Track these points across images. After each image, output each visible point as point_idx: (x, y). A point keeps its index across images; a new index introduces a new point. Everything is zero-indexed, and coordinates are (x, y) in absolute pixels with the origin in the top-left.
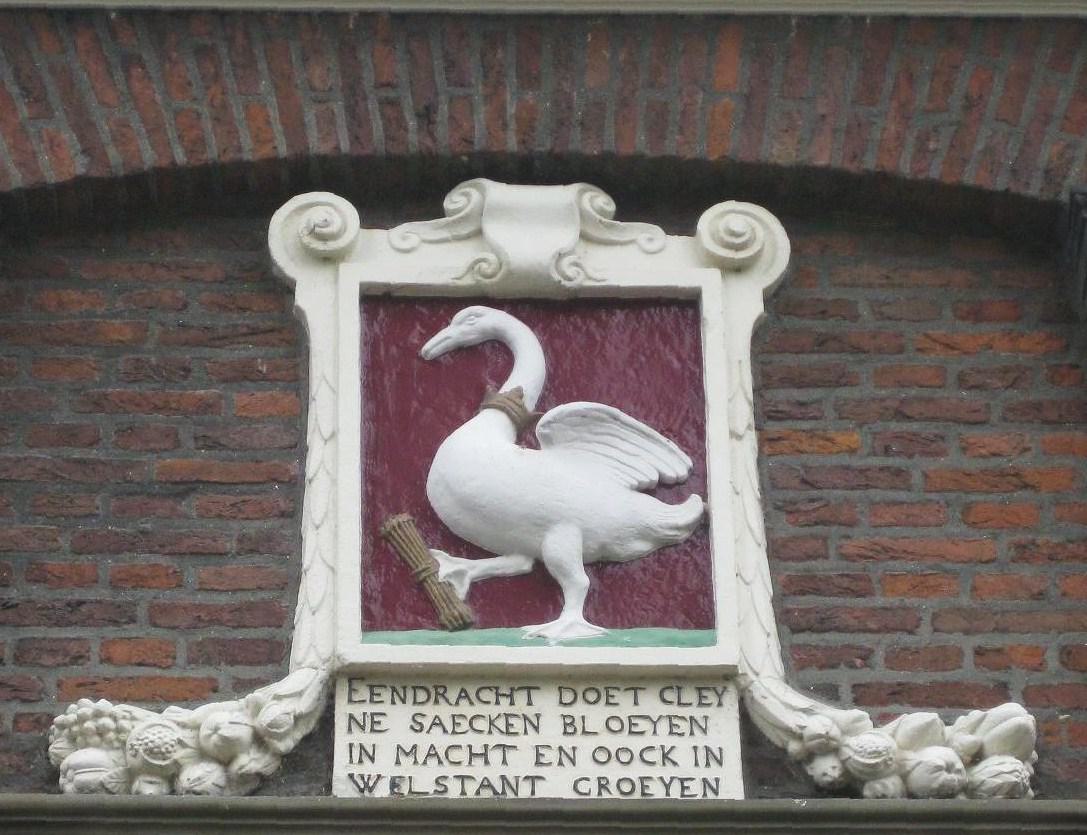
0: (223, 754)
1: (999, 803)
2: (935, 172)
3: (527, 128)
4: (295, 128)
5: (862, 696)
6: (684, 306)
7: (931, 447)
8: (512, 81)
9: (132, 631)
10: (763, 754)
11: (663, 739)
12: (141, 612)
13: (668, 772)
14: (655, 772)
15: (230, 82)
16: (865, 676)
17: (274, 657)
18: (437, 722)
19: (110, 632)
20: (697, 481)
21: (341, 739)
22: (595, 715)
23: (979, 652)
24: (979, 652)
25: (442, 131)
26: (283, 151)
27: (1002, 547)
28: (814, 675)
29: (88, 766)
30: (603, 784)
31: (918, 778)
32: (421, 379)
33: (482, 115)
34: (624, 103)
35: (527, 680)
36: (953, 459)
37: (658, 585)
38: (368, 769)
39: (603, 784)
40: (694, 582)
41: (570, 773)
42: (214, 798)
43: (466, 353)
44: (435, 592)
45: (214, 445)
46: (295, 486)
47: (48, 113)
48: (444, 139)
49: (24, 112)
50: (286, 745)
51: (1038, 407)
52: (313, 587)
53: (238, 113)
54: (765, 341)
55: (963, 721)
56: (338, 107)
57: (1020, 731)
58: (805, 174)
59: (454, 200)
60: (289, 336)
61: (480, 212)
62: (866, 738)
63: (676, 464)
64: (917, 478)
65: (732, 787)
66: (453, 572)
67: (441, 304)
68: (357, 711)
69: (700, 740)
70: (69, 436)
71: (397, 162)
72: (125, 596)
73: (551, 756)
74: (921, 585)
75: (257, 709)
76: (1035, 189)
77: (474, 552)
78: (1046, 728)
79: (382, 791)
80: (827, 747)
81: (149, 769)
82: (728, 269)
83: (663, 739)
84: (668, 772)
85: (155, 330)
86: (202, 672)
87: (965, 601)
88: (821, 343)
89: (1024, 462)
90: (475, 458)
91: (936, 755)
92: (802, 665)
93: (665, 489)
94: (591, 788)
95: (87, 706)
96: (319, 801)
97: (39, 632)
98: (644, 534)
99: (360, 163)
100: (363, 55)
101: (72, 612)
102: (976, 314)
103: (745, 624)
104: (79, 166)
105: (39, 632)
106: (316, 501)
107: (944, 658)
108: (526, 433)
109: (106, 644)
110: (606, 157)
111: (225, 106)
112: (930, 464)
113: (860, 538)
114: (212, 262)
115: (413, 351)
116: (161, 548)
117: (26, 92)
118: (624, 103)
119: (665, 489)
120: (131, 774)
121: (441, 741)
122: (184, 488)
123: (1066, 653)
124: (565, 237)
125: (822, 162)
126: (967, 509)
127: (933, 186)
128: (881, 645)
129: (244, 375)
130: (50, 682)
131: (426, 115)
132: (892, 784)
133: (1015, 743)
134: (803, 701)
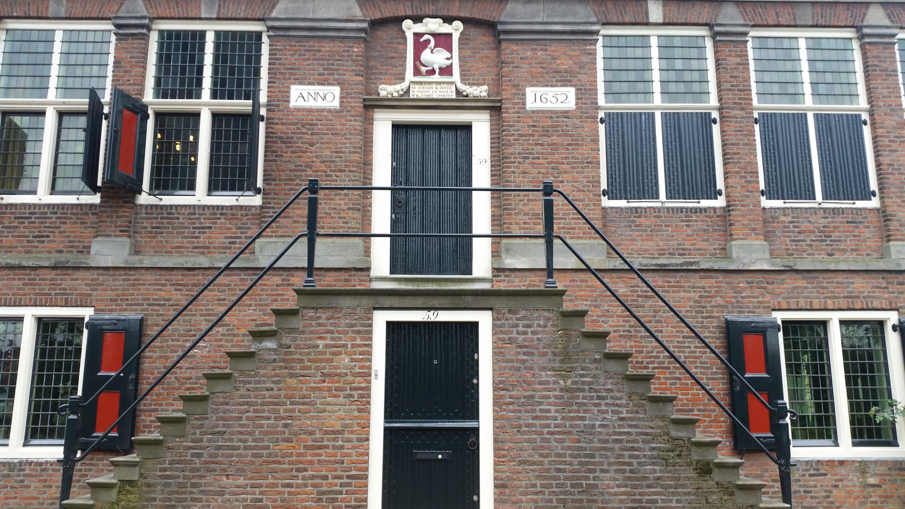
4: (405, 11)
5: (469, 84)
6: (451, 35)
7: (478, 53)
10: (458, 92)
17: (403, 79)
22: (439, 87)
29: (383, 93)
32: (420, 45)
35: (431, 83)
37: (446, 71)
43: (425, 41)
46: (405, 58)
48: (423, 13)
54: (460, 39)
60: (405, 38)
63: (449, 56)
65: (454, 96)
66: (423, 69)
67: (422, 35)
70: (379, 51)
76: (492, 20)
82: (456, 29)
90: (426, 55)
93: (448, 59)
101: (380, 74)
103: (456, 76)
104: (380, 16)
107: (478, 80)
114: (395, 28)
119: (448, 59)
129: (399, 43)
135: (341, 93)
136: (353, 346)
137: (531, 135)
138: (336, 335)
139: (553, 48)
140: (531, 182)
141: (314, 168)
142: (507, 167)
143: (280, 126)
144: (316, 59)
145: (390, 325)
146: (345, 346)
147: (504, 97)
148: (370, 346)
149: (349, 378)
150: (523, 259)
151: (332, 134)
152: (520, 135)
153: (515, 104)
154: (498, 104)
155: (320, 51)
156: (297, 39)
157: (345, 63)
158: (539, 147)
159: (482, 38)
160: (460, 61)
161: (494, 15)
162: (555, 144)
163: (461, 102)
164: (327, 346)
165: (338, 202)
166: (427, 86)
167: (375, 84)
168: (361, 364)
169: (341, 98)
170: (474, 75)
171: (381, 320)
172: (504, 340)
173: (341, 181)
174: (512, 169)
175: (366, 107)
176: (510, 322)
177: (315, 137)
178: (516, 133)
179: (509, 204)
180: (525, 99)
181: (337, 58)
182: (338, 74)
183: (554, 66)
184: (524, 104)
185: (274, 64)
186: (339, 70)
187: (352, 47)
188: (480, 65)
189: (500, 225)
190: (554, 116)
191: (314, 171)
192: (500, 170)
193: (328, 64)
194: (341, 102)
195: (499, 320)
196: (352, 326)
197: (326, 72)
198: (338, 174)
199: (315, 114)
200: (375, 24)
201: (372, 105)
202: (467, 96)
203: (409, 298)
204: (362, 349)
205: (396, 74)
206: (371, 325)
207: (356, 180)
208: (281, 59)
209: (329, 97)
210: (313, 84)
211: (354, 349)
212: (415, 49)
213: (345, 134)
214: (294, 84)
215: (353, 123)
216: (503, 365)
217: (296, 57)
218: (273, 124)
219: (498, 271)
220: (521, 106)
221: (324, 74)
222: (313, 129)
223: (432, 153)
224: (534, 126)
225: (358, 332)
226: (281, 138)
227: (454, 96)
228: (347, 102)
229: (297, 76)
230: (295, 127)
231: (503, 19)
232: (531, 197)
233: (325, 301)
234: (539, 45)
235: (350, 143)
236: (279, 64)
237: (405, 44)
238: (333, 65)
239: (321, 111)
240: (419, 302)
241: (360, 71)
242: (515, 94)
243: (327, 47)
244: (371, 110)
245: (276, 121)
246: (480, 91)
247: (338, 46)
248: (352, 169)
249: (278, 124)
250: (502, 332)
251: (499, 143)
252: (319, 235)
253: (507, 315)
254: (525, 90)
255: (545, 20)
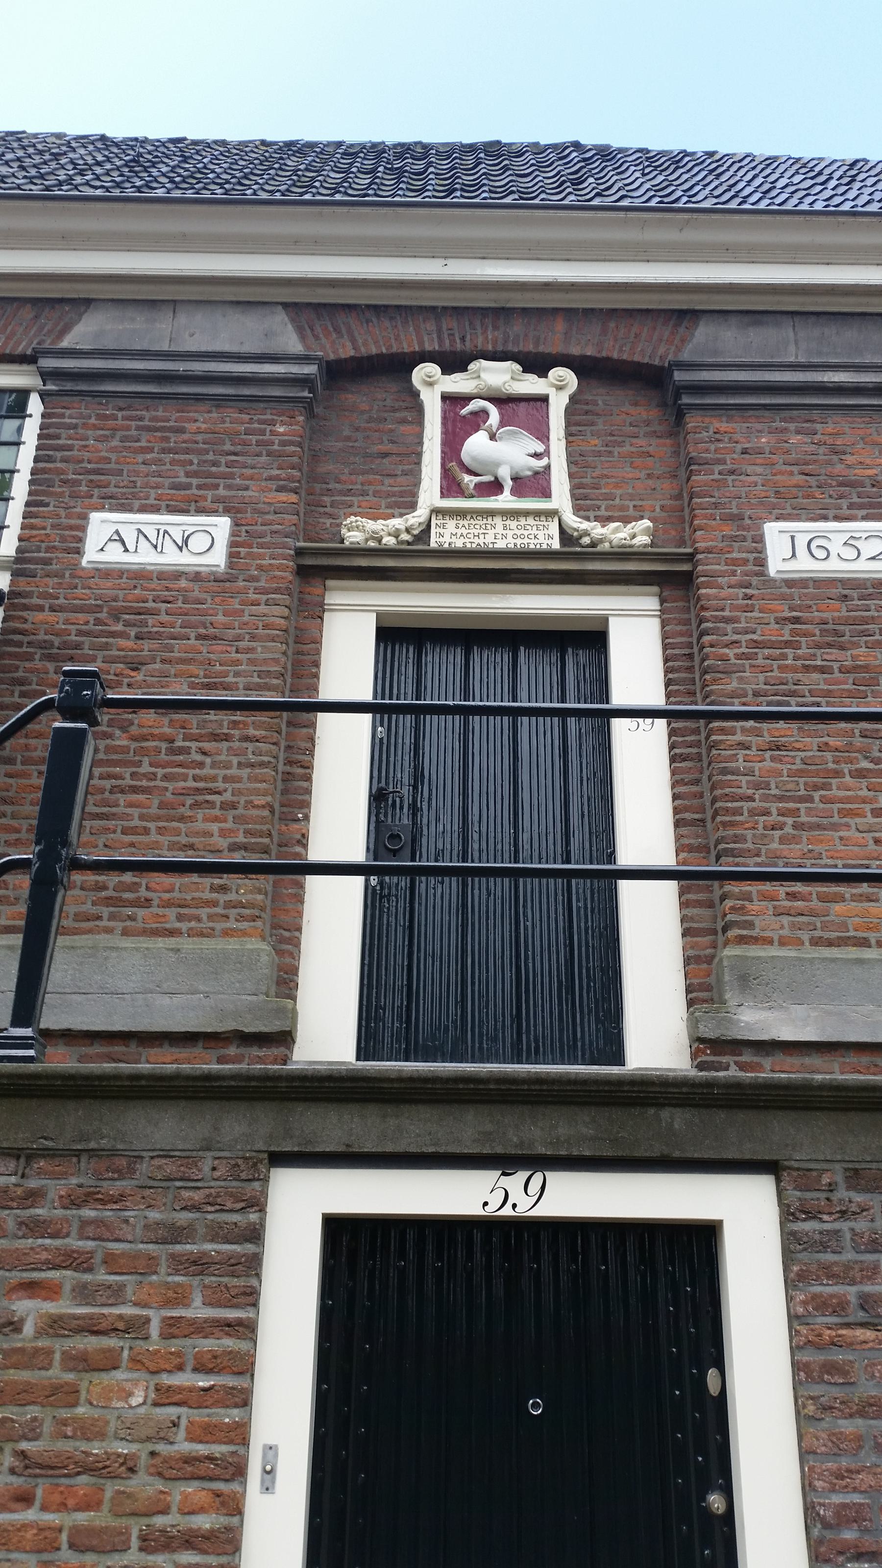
0: (396, 534)
1: (641, 549)
2: (625, 357)
3: (495, 342)
4: (421, 343)
5: (597, 519)
6: (544, 399)
7: (620, 444)
8: (490, 328)
9: (367, 498)
10: (565, 535)
11: (534, 531)
12: (370, 493)
13: (536, 541)
14: (532, 541)
15: (400, 328)
16: (598, 513)
17: (412, 506)
18: (463, 526)
19: (361, 498)
20: (547, 453)
21: (433, 530)
22: (513, 524)
23: (634, 506)
24: (634, 506)
25: (468, 343)
26: (417, 349)
27: (643, 475)
28: (582, 513)
29: (353, 537)
30: (515, 545)
31: (615, 542)
32: (460, 421)
33: (480, 339)
34: (526, 335)
35: (491, 513)
36: (627, 448)
37: (533, 484)
38: (441, 539)
39: (515, 545)
40: (545, 484)
41: (505, 542)
42: (394, 547)
44: (463, 486)
45: (393, 442)
46: (419, 455)
47: (342, 337)
48: (469, 346)
49: (334, 336)
50: (416, 532)
51: (655, 432)
52: (425, 484)
53: (402, 337)
54: (569, 412)
55: (630, 526)
56: (435, 336)
57: (649, 527)
58: (584, 357)
59: (471, 367)
60: (418, 409)
61: (479, 369)
62: (597, 530)
63: (540, 448)
64: (616, 454)
65: (556, 545)
67: (466, 399)
68: (438, 522)
69: (546, 531)
70: (348, 439)
71: (454, 353)
72: (366, 488)
73: (499, 536)
74: (617, 486)
75: (407, 520)
76: (657, 362)
77: (476, 475)
78: (656, 529)
79: (446, 546)
80: (586, 533)
81: (373, 538)
82: (559, 387)
83: (534, 531)
84: (536, 541)
85: (376, 407)
86: (390, 511)
87: (630, 491)
88: (587, 413)
89: (650, 449)
90: (477, 445)
91: (621, 535)
92: (578, 510)
93: (537, 456)
94: (511, 546)
95: (353, 518)
96: (426, 547)
97: (338, 498)
98: (530, 469)
99: (440, 353)
100: (443, 320)
102: (636, 404)
103: (561, 496)
104: (352, 353)
105: (338, 498)
106: (426, 458)
107: (623, 508)
108: (493, 437)
109: (359, 501)
110: (519, 352)
111: (398, 335)
112: (620, 449)
113: (597, 472)
114: (393, 387)
115: (457, 414)
116: (377, 473)
117: (335, 330)
118: (526, 335)
119: (537, 456)
120: (367, 540)
121: (465, 532)
122: (385, 455)
123: (662, 507)
124: (507, 377)
125: (589, 354)
126: (632, 463)
127: (624, 362)
128: (603, 504)
129: (404, 421)
130: (342, 513)
131: (463, 339)
132: (607, 545)
133: (646, 531)
134: (579, 520)
135: (233, 534)
136: (173, 1328)
137: (787, 644)
138: (102, 1276)
139: (830, 428)
140: (800, 773)
141: (134, 730)
142: (723, 731)
143: (40, 616)
144: (170, 451)
145: (339, 1232)
146: (134, 1328)
147: (700, 545)
148: (247, 1329)
149: (143, 1485)
150: (799, 1010)
151: (199, 637)
152: (756, 644)
153: (735, 562)
154: (686, 567)
155: (181, 430)
156: (121, 402)
157: (249, 461)
158: (815, 676)
159: (629, 410)
160: (570, 463)
161: (661, 351)
162: (866, 668)
163: (572, 565)
164: (55, 1326)
165: (200, 825)
166: (480, 522)
167: (331, 516)
168: (200, 1416)
169: (232, 544)
170: (610, 497)
171: (300, 1207)
172: (839, 1307)
173: (214, 765)
174: (739, 737)
175: (305, 573)
176: (861, 1225)
177: (146, 645)
178: (744, 638)
179: (737, 839)
180: (762, 551)
181: (228, 447)
182: (229, 487)
183: (839, 468)
184: (762, 562)
185: (49, 459)
186: (231, 476)
187: (273, 423)
188: (628, 472)
189: (711, 905)
190: (855, 594)
191: (134, 739)
192: (698, 744)
193: (201, 463)
194: (232, 556)
195: (812, 1215)
196: (176, 1234)
197: (195, 481)
198: (206, 746)
199: (155, 584)
200: (340, 373)
201: (324, 568)
202: (593, 545)
203: (425, 1112)
204: (208, 1344)
205: (389, 495)
206: (255, 1235)
207: (262, 765)
208: (70, 448)
209: (199, 543)
210: (155, 510)
211: (174, 1346)
212: (445, 432)
213: (238, 639)
214: (101, 508)
215: (263, 609)
216: (848, 1426)
217: (115, 443)
218: (26, 608)
219: (707, 1046)
220: (750, 567)
221: (188, 487)
222: (145, 624)
223: (491, 688)
224: (796, 620)
225: (199, 1265)
226: (44, 645)
227: (556, 545)
228: (249, 555)
229: (112, 490)
230: (91, 618)
231: (686, 356)
232: (804, 819)
233: (69, 1122)
234: (792, 420)
235: (251, 662)
236: (64, 460)
237: (419, 420)
238: (215, 464)
239: (170, 576)
240: (466, 1129)
241: (289, 479)
242: (734, 539)
243: (201, 420)
244: (317, 582)
245: (35, 601)
246: (636, 533)
247: (232, 420)
248: (252, 732)
249: (41, 608)
250: (829, 1273)
251: (690, 669)
252: (77, 865)
253: (842, 1193)
254: (760, 528)
255: (802, 359)
